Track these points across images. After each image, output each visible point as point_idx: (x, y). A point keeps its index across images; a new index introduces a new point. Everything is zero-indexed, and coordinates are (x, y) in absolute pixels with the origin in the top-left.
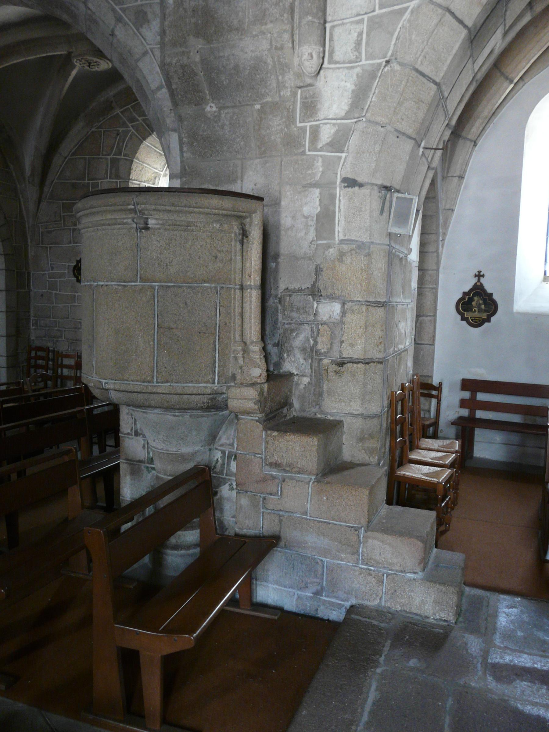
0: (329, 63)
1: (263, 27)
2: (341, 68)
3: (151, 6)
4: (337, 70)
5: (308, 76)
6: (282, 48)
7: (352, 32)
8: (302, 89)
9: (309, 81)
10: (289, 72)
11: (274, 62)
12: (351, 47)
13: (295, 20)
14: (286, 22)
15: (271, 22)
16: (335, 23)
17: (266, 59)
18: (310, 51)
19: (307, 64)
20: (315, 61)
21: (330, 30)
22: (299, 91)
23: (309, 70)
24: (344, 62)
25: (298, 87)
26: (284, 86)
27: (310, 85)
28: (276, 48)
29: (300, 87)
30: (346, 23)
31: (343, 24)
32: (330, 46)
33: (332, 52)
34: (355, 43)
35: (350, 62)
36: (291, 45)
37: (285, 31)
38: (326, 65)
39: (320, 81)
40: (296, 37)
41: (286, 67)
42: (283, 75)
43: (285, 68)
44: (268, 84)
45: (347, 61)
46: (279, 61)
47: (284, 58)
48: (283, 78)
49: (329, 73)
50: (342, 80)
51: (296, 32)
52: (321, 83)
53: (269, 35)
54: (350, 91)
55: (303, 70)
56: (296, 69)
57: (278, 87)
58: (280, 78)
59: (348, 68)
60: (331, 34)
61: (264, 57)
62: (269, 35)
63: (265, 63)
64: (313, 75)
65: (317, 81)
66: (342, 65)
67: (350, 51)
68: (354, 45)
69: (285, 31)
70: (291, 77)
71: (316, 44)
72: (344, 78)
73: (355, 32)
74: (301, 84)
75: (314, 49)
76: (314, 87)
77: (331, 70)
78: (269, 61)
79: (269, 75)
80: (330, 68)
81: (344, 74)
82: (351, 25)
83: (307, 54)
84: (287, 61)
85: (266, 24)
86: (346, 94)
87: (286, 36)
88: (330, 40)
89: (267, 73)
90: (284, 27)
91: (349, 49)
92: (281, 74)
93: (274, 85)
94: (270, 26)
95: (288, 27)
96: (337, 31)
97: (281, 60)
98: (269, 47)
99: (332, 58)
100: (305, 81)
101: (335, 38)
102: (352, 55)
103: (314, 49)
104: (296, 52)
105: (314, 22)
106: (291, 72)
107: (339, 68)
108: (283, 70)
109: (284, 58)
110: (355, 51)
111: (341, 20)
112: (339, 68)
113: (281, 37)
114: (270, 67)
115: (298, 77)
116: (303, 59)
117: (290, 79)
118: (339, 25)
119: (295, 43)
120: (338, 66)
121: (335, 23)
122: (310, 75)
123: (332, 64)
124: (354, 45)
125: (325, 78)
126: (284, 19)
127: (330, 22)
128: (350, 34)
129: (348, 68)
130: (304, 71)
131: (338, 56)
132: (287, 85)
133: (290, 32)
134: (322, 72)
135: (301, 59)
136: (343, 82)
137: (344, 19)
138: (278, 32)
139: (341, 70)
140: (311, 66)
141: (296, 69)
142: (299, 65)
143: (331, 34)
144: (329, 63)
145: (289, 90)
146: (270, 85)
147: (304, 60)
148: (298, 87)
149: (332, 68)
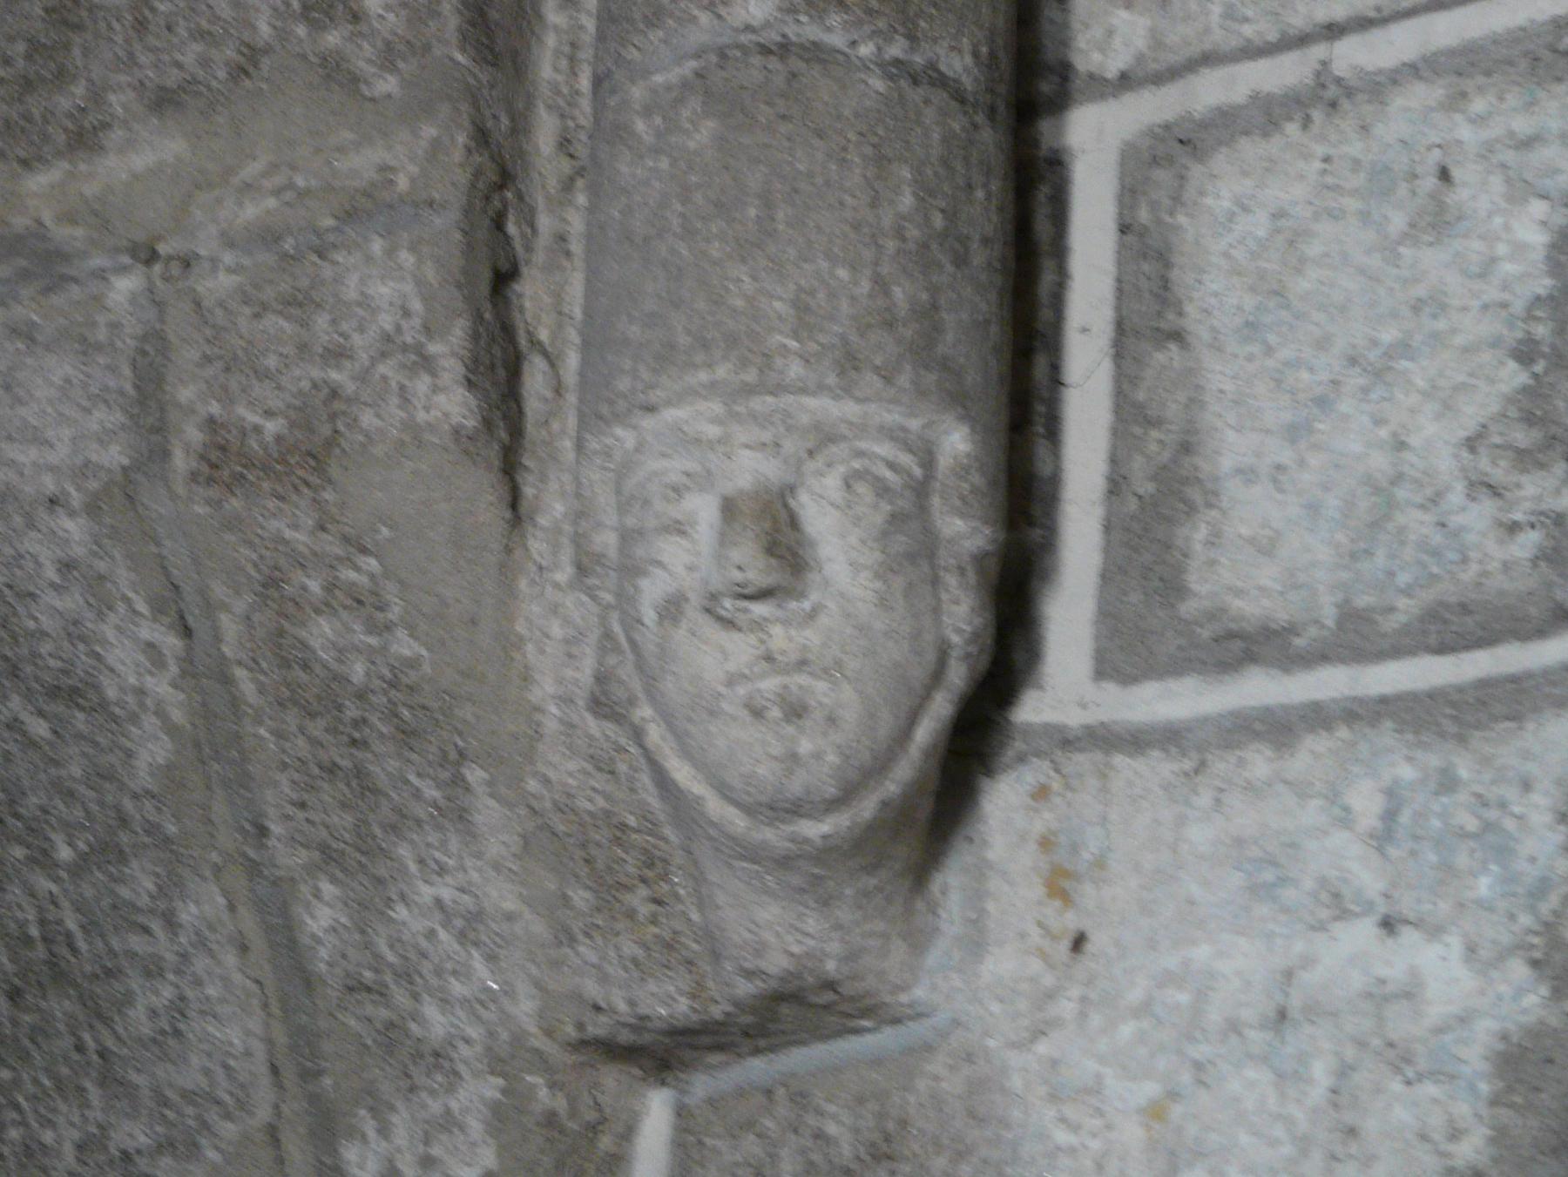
0: (1120, 658)
1: (39, 181)
2: (1317, 717)
3: (800, 1099)
4: (1259, 762)
5: (752, 853)
6: (311, 454)
7: (1477, 191)
8: (702, 1085)
9: (773, 932)
10: (457, 815)
11: (204, 673)
12: (1473, 412)
13: (546, 68)
14: (387, 85)
15: (164, 101)
16: (1210, 91)
17: (75, 631)
18: (749, 468)
19: (712, 657)
20: (852, 640)
21: (1129, 193)
22: (656, 1113)
23: (753, 750)
24: (1357, 638)
25: (612, 1051)
26: (392, 1035)
27: (794, 1009)
28: (225, 462)
29: (660, 1054)
30: (1379, 86)
31: (1326, 97)
32: (1131, 415)
33: (1159, 505)
34: (1525, 353)
35: (1449, 628)
36: (451, 403)
37: (364, 209)
38: (1066, 682)
39: (976, 943)
40: (550, 301)
41: (407, 736)
42: (359, 860)
43: (384, 765)
44: (138, 1018)
45: (1407, 608)
46: (285, 652)
47: (365, 603)
48: (369, 908)
49: (1126, 814)
50: (1338, 904)
51: (556, 219)
52: (1001, 964)
53: (125, 286)
54: (1474, 1054)
55: (663, 781)
56: (562, 768)
57: (300, 1057)
58: (322, 917)
59: (1415, 714)
60: (1147, 252)
61: (56, 606)
62: (125, 286)
63: (72, 693)
64: (815, 830)
65: (918, 941)
66: (1329, 683)
67: (1446, 463)
68: (1513, 376)
69: (364, 209)
70: (502, 896)
71: (849, 363)
72: (1368, 878)
73: (1521, 190)
74: (666, 1000)
75: (824, 437)
76: (883, 1039)
77: (1157, 768)
78: (132, 655)
79: (141, 881)
80: (1136, 741)
81: (1365, 802)
82: (1456, 101)
83: (704, 509)
84: (404, 646)
85: (84, 139)
86: (1397, 1109)
87: (394, 286)
88: (1122, 330)
89: (106, 854)
90: (362, 163)
91: (1437, 442)
92: (329, 858)
93: (235, 1031)
94: (142, 155)
95: (418, 155)
96: (1235, 212)
97: (321, 633)
98: (114, 456)
99: (1172, 588)
100: (712, 941)
101: (1214, 294)
102: (1477, 517)
103: (824, 437)
104: (551, 504)
105: (816, 53)
106: (486, 811)
107: (1278, 728)
108: (365, 786)
109: (365, 603)
110: (1525, 459)
111: (1302, 40)
112: (1278, 728)
113: (299, 304)
114: (153, 751)
115: (608, 889)
116: (652, 590)
117: (469, 924)
118: (1269, 114)
119: (535, 379)
120: (1260, 688)
121: (1210, 91)
122: (772, 836)
123: (1176, 667)
124: (1513, 376)
125: (1060, 885)
126: (363, 58)
127: (1126, 82)
128: (1437, 221)
129: (1415, 714)
130: (682, 773)
131: (1267, 540)
132: (436, 1022)
133: (445, 222)
134: (1004, 801)
135: (626, 602)
136: (1361, 934)
137: (1334, 31)
138: (267, 236)
139: (1313, 754)
140: (788, 682)
141: (562, 768)
142: (604, 704)
143: (1147, 252)
144: (1120, 658)
145: (477, 1092)
146: (169, 1036)
147: (672, 609)
148: (612, 1051)
149: (1170, 737)
